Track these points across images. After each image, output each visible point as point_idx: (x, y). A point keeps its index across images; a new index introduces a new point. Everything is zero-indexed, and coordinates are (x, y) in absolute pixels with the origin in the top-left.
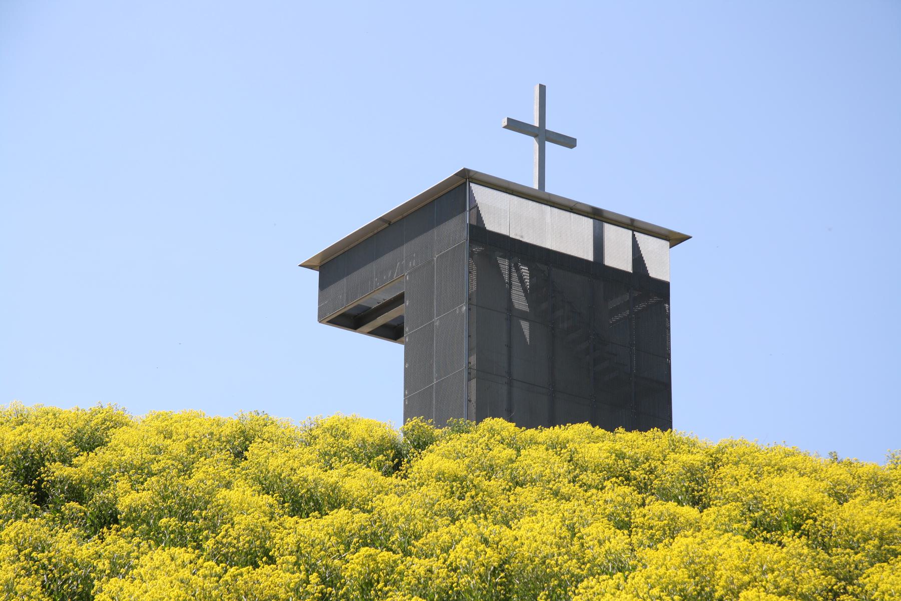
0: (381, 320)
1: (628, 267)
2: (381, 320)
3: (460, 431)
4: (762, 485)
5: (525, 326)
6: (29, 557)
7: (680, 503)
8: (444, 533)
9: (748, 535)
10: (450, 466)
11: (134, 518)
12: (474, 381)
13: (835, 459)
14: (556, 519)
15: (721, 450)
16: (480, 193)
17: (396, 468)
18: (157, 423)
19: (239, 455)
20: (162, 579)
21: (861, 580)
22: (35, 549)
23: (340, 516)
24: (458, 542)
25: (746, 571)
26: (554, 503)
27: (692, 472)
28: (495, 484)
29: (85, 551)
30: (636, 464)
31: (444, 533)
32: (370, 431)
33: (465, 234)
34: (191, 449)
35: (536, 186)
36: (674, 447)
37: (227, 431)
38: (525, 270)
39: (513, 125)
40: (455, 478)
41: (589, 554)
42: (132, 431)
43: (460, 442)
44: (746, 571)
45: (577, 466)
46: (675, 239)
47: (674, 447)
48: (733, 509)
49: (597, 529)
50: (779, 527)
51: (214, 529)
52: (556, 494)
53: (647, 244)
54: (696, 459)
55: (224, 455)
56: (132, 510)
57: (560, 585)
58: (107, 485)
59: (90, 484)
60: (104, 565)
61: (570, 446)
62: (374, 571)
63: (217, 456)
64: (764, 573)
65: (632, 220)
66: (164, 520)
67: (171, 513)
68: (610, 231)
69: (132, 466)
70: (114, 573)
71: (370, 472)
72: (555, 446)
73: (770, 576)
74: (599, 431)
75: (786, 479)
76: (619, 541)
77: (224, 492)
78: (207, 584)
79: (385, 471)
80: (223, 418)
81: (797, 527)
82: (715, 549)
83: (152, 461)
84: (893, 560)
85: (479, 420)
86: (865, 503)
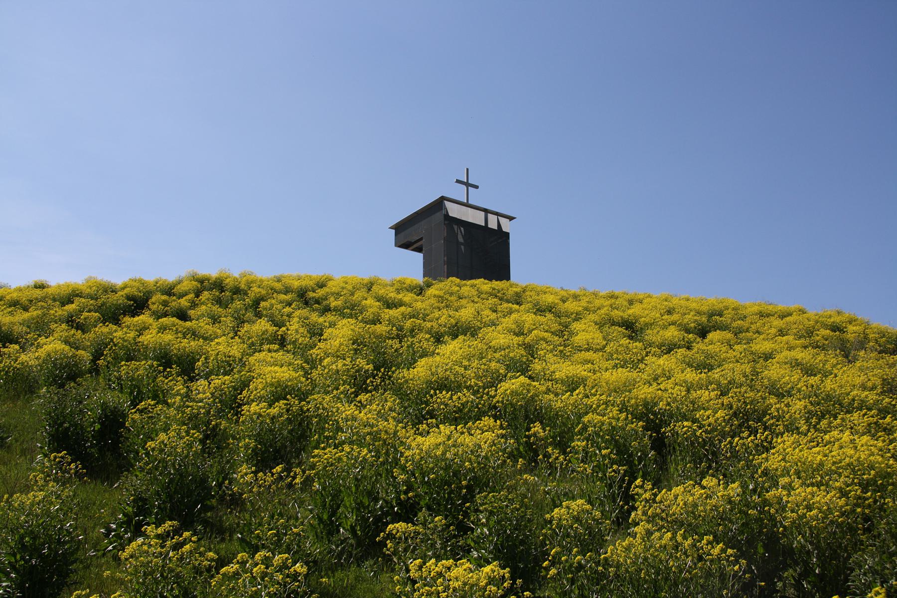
0: (415, 246)
1: (496, 228)
2: (415, 246)
3: (442, 281)
4: (539, 298)
5: (462, 247)
6: (303, 322)
7: (513, 304)
8: (437, 314)
9: (535, 313)
10: (437, 293)
11: (336, 309)
12: (446, 266)
13: (562, 289)
14: (473, 309)
15: (526, 287)
16: (448, 204)
17: (421, 293)
18: (343, 279)
19: (369, 290)
20: (345, 328)
21: (570, 327)
22: (305, 319)
23: (403, 309)
24: (441, 317)
25: (534, 325)
26: (472, 304)
27: (517, 294)
28: (453, 298)
29: (321, 320)
30: (499, 292)
31: (437, 314)
32: (412, 282)
33: (442, 218)
34: (354, 288)
35: (466, 202)
36: (511, 286)
37: (365, 282)
38: (462, 229)
39: (458, 181)
40: (440, 297)
41: (484, 320)
42: (335, 282)
43: (441, 285)
44: (534, 325)
45: (480, 293)
46: (511, 218)
47: (511, 286)
48: (530, 305)
49: (487, 312)
50: (544, 311)
51: (362, 313)
52: (473, 301)
53: (502, 220)
54: (518, 290)
55: (364, 289)
56: (335, 307)
57: (474, 330)
58: (327, 299)
59: (322, 299)
60: (327, 324)
61: (477, 286)
62: (415, 326)
63: (362, 290)
64: (540, 325)
65: (497, 213)
66: (345, 310)
67: (348, 308)
68: (490, 216)
69: (335, 293)
70: (330, 327)
71: (412, 295)
72: (473, 286)
73: (542, 326)
74: (486, 281)
75: (547, 295)
76: (493, 316)
77: (365, 301)
78: (360, 330)
79: (517, 304)
80: (364, 278)
81: (550, 311)
82: (524, 318)
83: (341, 292)
84: (580, 320)
85: (448, 278)
86: (571, 303)
